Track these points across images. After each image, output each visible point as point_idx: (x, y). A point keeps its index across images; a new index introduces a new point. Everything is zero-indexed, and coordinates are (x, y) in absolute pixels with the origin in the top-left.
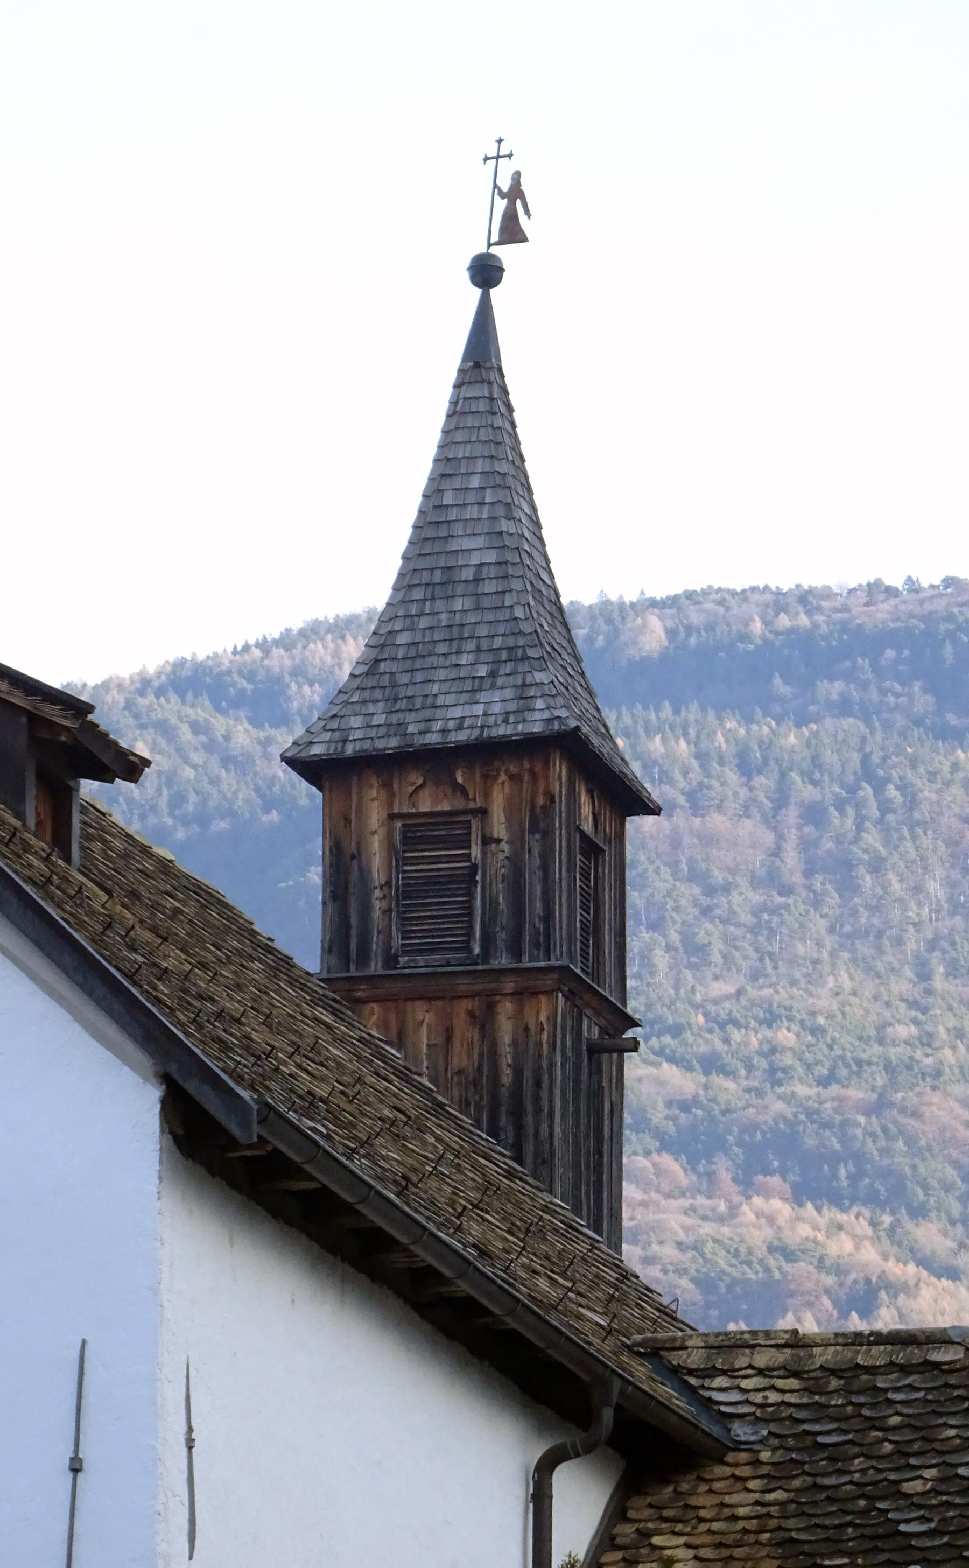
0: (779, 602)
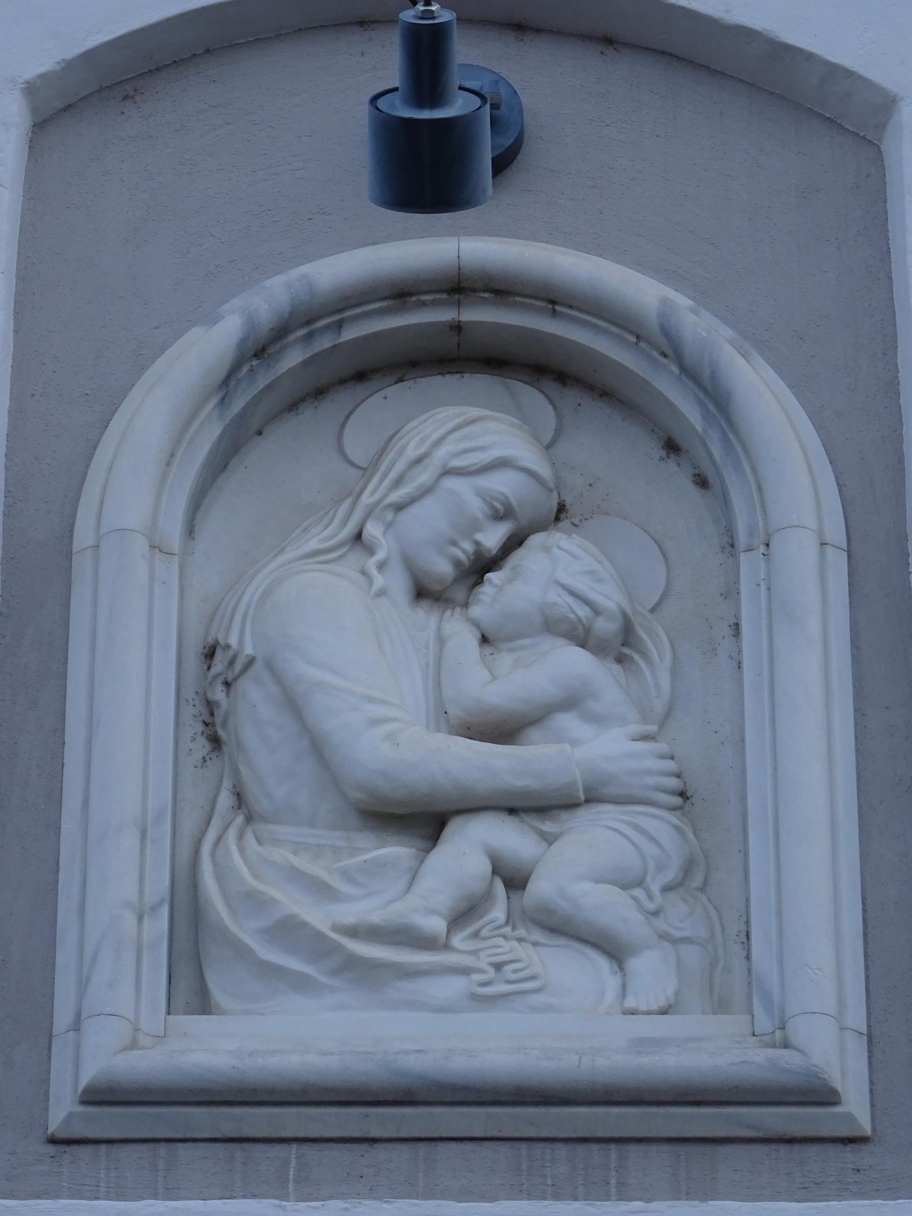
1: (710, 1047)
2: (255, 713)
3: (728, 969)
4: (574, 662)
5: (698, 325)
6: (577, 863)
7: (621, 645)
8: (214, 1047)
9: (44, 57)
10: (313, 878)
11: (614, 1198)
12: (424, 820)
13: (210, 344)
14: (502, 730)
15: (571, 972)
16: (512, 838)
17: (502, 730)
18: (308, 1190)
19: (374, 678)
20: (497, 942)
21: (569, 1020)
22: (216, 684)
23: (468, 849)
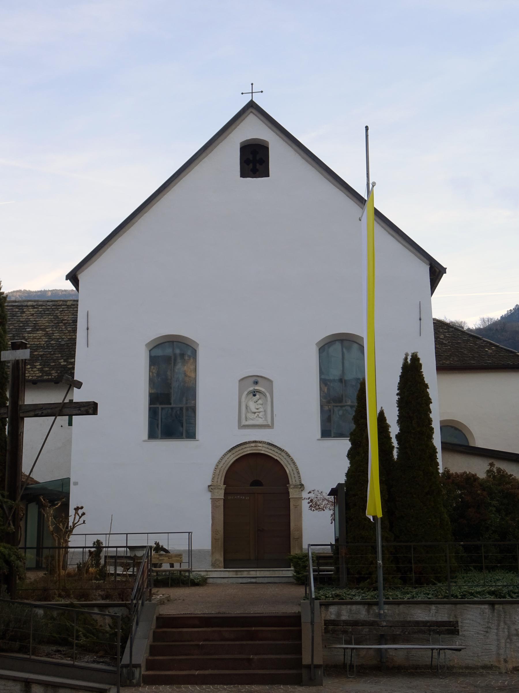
0: (62, 291)
1: (265, 423)
2: (248, 408)
3: (266, 420)
4: (260, 406)
5: (265, 392)
6: (261, 415)
7: (262, 404)
8: (247, 423)
9: (239, 379)
10: (250, 416)
11: (142, 685)
12: (255, 413)
13: (246, 393)
14: (257, 409)
15: (260, 419)
16: (258, 414)
17: (257, 409)
18: (309, 167)
19: (253, 406)
20: (257, 418)
21: (260, 422)
22: (247, 407)
23: (256, 414)
